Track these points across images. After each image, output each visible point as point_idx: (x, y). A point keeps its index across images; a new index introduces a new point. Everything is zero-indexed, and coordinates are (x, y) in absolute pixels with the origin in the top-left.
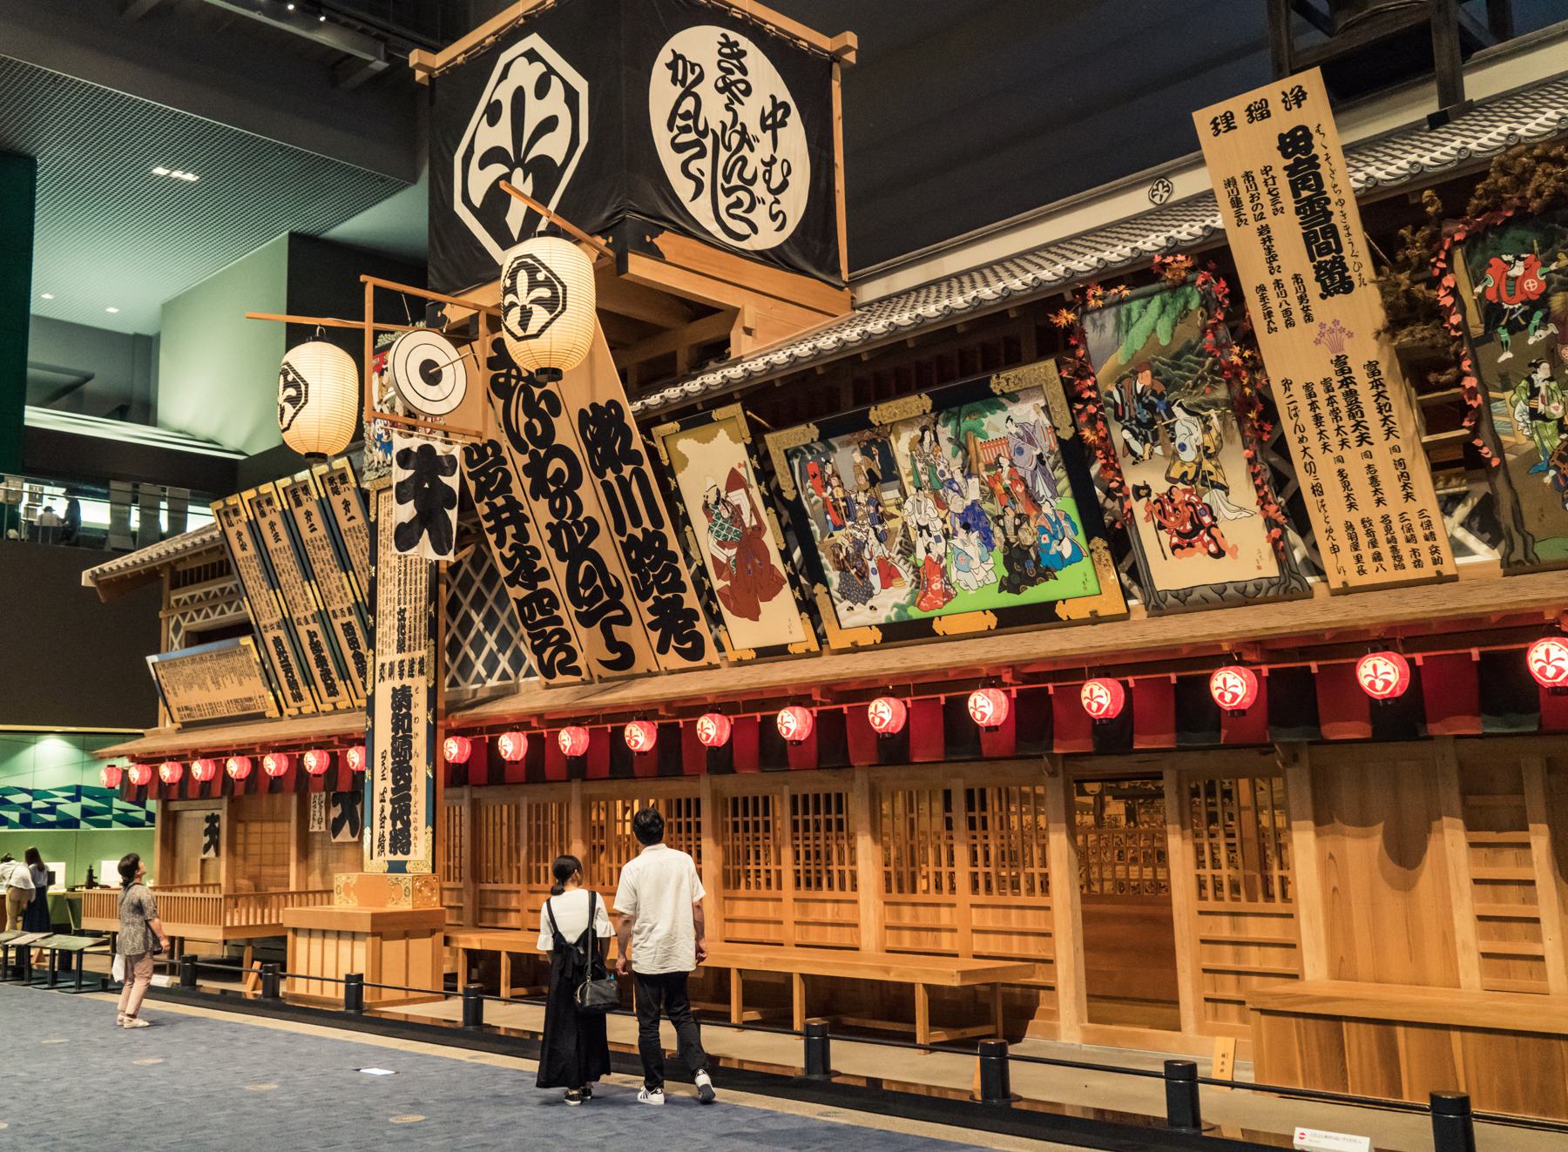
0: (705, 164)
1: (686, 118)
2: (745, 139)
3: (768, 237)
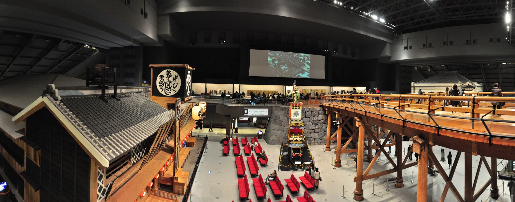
0: (164, 87)
1: (162, 83)
2: (170, 82)
3: (173, 93)
